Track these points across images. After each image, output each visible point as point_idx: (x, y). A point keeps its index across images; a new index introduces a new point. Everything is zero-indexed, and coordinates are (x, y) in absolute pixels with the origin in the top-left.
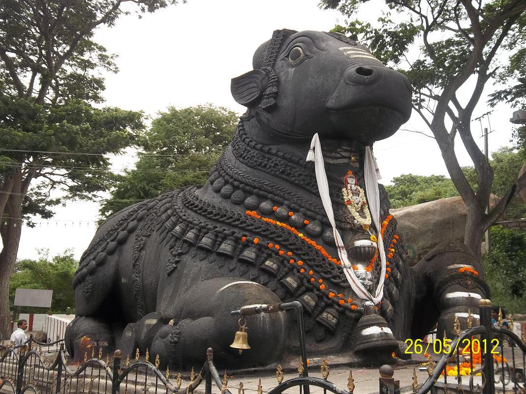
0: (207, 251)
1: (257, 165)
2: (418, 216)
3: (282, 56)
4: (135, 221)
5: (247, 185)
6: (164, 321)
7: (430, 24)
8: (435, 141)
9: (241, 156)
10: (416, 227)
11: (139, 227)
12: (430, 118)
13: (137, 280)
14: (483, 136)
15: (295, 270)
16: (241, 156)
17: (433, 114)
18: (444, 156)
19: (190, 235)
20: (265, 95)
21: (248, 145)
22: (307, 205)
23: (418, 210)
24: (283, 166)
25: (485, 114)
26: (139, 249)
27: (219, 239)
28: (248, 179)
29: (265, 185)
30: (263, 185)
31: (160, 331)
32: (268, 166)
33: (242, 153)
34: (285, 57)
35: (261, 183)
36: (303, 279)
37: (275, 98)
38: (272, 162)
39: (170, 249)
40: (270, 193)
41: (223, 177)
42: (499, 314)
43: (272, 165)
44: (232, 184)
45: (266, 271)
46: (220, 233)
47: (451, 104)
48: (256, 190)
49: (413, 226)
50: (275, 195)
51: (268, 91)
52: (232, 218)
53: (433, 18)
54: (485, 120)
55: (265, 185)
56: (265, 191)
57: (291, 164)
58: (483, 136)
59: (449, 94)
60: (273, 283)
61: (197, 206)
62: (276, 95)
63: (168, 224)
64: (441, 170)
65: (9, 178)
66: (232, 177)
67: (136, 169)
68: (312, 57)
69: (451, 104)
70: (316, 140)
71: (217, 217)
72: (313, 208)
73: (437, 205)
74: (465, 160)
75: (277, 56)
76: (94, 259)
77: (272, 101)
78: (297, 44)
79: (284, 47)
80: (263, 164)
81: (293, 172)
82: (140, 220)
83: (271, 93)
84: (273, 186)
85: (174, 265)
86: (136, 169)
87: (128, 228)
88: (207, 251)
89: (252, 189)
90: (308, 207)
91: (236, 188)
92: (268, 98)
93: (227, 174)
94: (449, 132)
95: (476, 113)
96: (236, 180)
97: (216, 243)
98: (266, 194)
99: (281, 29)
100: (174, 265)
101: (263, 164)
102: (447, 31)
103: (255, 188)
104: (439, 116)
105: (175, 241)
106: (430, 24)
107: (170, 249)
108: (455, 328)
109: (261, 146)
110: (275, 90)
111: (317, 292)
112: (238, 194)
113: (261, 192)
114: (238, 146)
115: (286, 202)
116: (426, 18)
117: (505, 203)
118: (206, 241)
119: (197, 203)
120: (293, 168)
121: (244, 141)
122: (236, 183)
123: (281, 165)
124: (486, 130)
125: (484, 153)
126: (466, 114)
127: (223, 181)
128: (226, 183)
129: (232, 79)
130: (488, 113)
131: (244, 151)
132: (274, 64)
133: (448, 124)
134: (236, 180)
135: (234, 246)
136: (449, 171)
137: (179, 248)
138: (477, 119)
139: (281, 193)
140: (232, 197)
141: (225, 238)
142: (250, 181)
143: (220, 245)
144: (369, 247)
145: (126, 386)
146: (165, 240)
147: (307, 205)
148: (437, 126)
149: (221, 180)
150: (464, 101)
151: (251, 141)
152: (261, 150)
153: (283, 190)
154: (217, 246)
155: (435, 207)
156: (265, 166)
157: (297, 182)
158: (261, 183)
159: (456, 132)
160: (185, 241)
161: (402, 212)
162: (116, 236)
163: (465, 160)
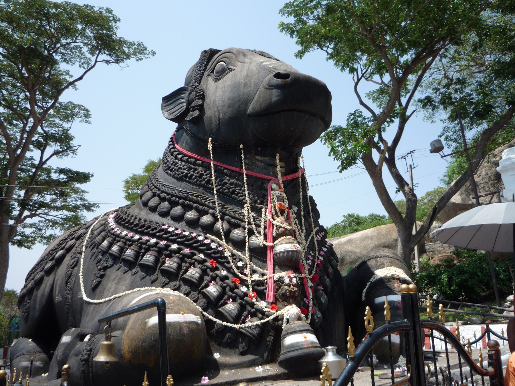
0: (148, 269)
1: (182, 176)
4: (74, 241)
5: (173, 196)
7: (359, 78)
9: (168, 169)
10: (357, 251)
11: (77, 245)
13: (68, 298)
14: (408, 172)
15: (218, 278)
19: (115, 248)
20: (191, 108)
21: (176, 158)
22: (231, 213)
24: (208, 176)
25: (408, 153)
26: (72, 266)
27: (143, 251)
28: (174, 190)
29: (190, 195)
30: (188, 195)
32: (117, 279)
33: (170, 165)
34: (211, 72)
35: (186, 193)
36: (226, 287)
38: (198, 173)
39: (97, 263)
40: (194, 202)
41: (151, 190)
43: (198, 175)
44: (159, 196)
48: (181, 201)
49: (355, 250)
53: (362, 73)
54: (409, 159)
55: (190, 195)
58: (408, 172)
61: (125, 220)
66: (159, 190)
67: (51, 175)
68: (234, 70)
72: (237, 215)
75: (203, 74)
78: (223, 59)
82: (78, 238)
84: (198, 196)
85: (99, 279)
86: (51, 175)
87: (66, 247)
88: (130, 264)
89: (177, 199)
90: (233, 215)
91: (163, 200)
93: (155, 187)
94: (377, 164)
96: (163, 192)
100: (99, 279)
103: (180, 198)
106: (359, 78)
107: (97, 263)
108: (366, 323)
111: (239, 301)
112: (166, 205)
114: (167, 159)
115: (211, 211)
118: (149, 258)
119: (125, 217)
121: (172, 155)
122: (163, 195)
123: (206, 175)
125: (384, 164)
126: (392, 150)
128: (154, 195)
131: (172, 164)
132: (200, 80)
135: (136, 251)
136: (386, 209)
137: (105, 262)
138: (403, 157)
139: (207, 203)
140: (158, 208)
141: (147, 250)
142: (177, 192)
143: (143, 257)
146: (95, 255)
147: (231, 213)
149: (156, 199)
151: (178, 154)
153: (204, 198)
154: (140, 258)
157: (309, 262)
158: (186, 193)
160: (111, 255)
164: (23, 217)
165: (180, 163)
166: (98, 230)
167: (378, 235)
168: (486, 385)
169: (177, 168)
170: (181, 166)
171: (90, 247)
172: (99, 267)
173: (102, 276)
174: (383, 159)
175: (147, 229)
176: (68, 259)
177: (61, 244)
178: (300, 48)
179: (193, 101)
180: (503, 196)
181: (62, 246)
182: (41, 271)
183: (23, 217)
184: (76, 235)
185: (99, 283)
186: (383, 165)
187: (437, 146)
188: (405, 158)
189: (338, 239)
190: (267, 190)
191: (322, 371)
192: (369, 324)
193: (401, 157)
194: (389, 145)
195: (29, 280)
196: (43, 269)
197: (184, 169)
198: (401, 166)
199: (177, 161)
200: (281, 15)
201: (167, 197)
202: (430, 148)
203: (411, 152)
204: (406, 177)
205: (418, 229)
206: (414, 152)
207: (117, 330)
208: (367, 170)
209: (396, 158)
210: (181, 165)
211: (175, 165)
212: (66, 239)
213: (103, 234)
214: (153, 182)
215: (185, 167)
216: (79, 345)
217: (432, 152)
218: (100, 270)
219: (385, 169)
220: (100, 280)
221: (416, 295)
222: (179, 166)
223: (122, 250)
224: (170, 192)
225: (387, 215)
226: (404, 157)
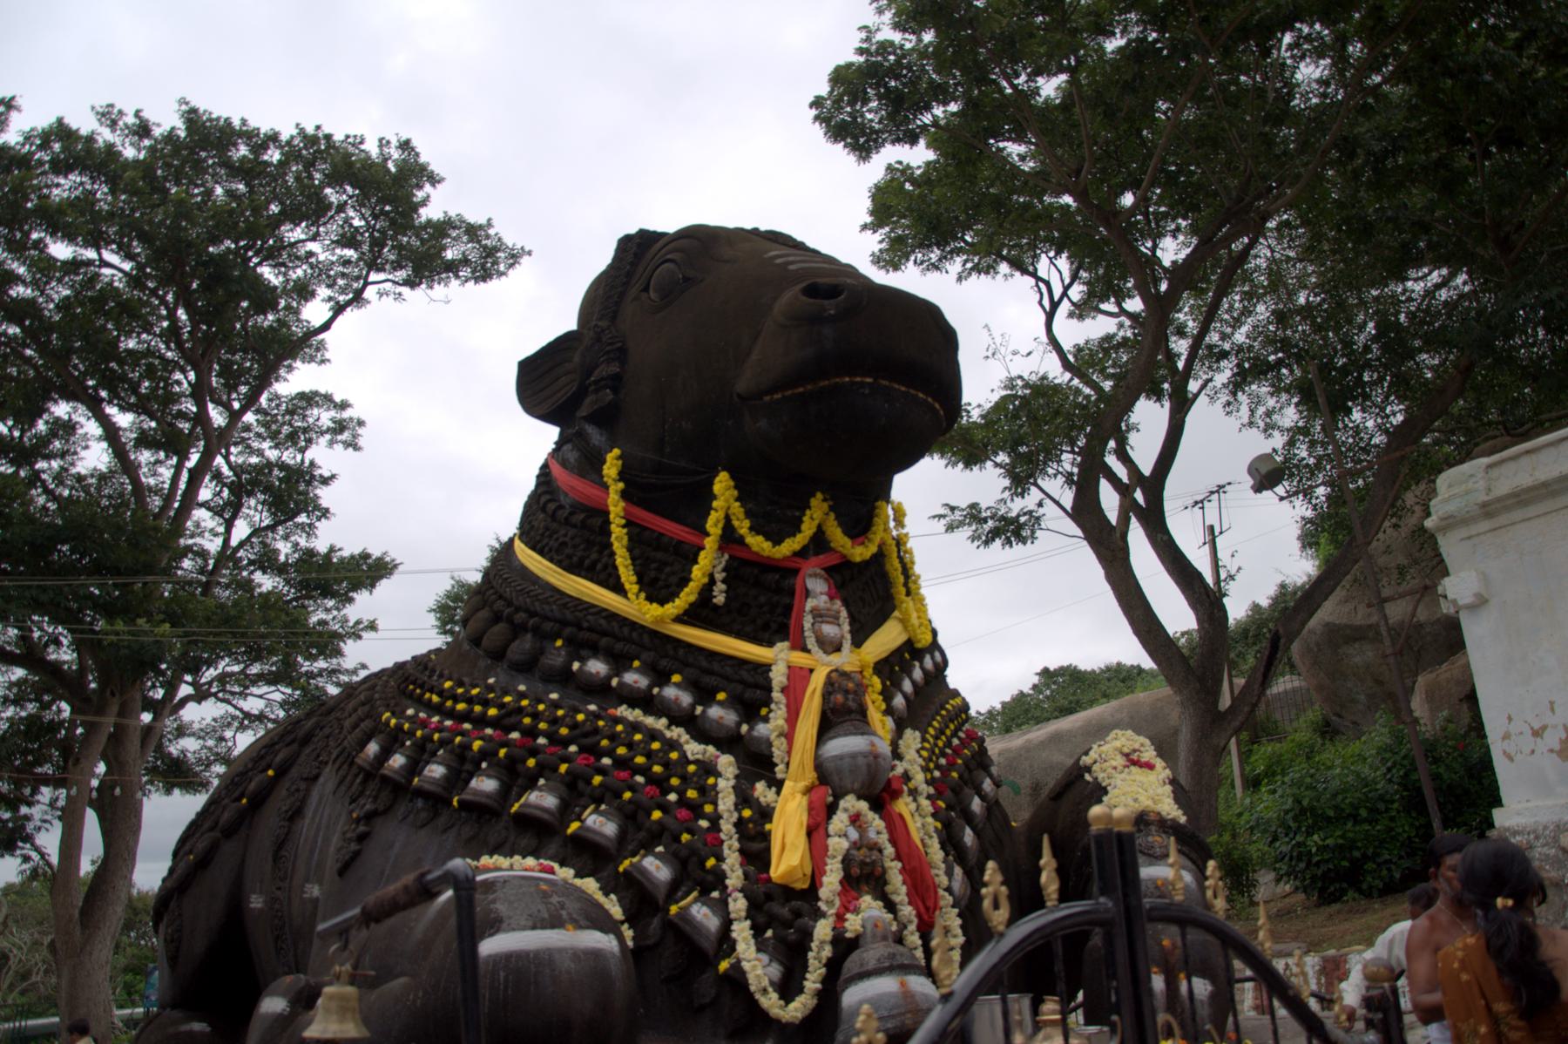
3: (633, 291)
4: (295, 746)
7: (1056, 298)
18: (1110, 578)
23: (1079, 724)
25: (1212, 493)
28: (548, 603)
32: (599, 566)
37: (615, 390)
40: (604, 634)
42: (1260, 922)
50: (618, 639)
54: (1211, 508)
56: (590, 629)
57: (659, 555)
62: (616, 382)
64: (1131, 652)
65: (108, 693)
66: (509, 604)
70: (722, 484)
74: (1177, 616)
77: (608, 395)
78: (669, 257)
79: (640, 269)
80: (587, 562)
81: (663, 577)
83: (602, 379)
93: (501, 597)
94: (1114, 521)
98: (594, 636)
101: (587, 562)
102: (1101, 317)
105: (365, 781)
106: (1056, 298)
109: (582, 516)
110: (614, 368)
116: (1047, 284)
120: (666, 564)
126: (1155, 484)
128: (497, 618)
130: (1220, 487)
133: (1109, 500)
138: (1196, 503)
144: (865, 755)
148: (1086, 512)
149: (500, 628)
150: (1144, 449)
152: (584, 525)
158: (581, 611)
159: (1129, 519)
160: (386, 780)
161: (1042, 732)
163: (1177, 616)
164: (177, 698)
165: (563, 532)
166: (354, 717)
167: (1132, 718)
169: (556, 545)
170: (567, 539)
171: (334, 762)
172: (355, 815)
173: (362, 838)
174: (1128, 507)
176: (282, 792)
177: (262, 757)
178: (869, 219)
179: (597, 366)
180: (1445, 597)
182: (212, 829)
183: (177, 698)
184: (301, 733)
185: (356, 855)
186: (1131, 527)
187: (1264, 470)
188: (1202, 508)
189: (1024, 734)
190: (792, 593)
191: (858, 1025)
192: (996, 906)
193: (1191, 502)
194: (1146, 469)
195: (182, 853)
196: (217, 823)
198: (1186, 532)
199: (555, 525)
200: (310, 130)
203: (1220, 489)
204: (1199, 559)
206: (1227, 488)
207: (397, 976)
208: (1086, 538)
210: (565, 535)
211: (550, 536)
212: (273, 745)
214: (494, 584)
215: (577, 540)
217: (1258, 488)
218: (358, 820)
219: (1137, 538)
220: (357, 847)
221: (1131, 836)
222: (561, 540)
223: (414, 767)
224: (538, 609)
225: (1148, 663)
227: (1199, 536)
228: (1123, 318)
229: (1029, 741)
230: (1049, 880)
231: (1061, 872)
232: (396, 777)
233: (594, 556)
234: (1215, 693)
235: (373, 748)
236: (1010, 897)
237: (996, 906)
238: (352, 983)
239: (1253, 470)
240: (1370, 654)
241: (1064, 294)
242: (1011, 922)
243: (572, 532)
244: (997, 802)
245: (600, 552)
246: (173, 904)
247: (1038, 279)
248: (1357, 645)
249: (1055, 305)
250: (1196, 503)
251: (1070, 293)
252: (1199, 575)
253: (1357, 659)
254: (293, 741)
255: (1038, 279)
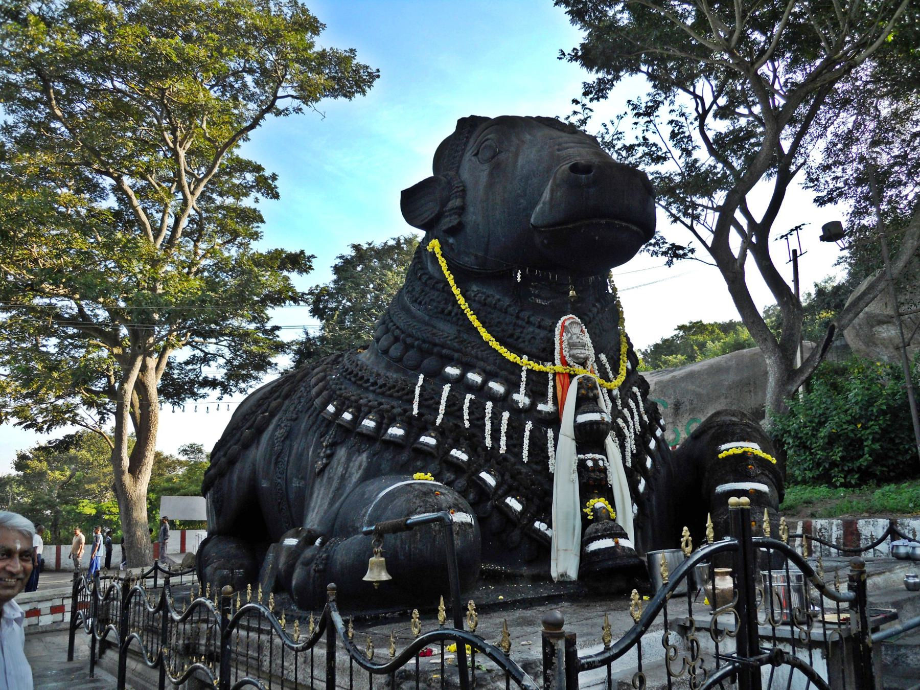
2: (706, 377)
6: (309, 540)
7: (707, 107)
8: (717, 270)
12: (709, 239)
16: (416, 301)
17: (712, 231)
18: (731, 290)
25: (792, 230)
31: (303, 556)
32: (453, 314)
37: (460, 215)
40: (457, 351)
45: (455, 465)
46: (387, 411)
47: (738, 215)
49: (698, 390)
51: (451, 204)
52: (403, 389)
54: (793, 239)
56: (449, 348)
59: (737, 199)
60: (461, 482)
63: (317, 402)
64: (730, 313)
69: (738, 215)
71: (383, 389)
73: (730, 359)
76: (225, 455)
80: (446, 311)
92: (451, 215)
93: (398, 328)
94: (736, 257)
95: (778, 228)
97: (382, 426)
99: (467, 116)
101: (446, 311)
103: (435, 345)
104: (721, 234)
106: (707, 107)
113: (444, 351)
116: (702, 99)
117: (820, 352)
119: (356, 370)
122: (409, 340)
124: (795, 251)
125: (749, 252)
126: (762, 229)
127: (392, 339)
128: (396, 339)
129: (402, 192)
133: (735, 241)
134: (410, 336)
138: (782, 237)
140: (404, 359)
145: (248, 637)
148: (719, 249)
154: (383, 431)
155: (730, 363)
156: (450, 313)
162: (254, 422)
168: (847, 687)
174: (747, 244)
175: (390, 389)
181: (265, 407)
192: (687, 546)
194: (758, 218)
197: (439, 302)
201: (416, 343)
202: (822, 234)
203: (797, 228)
205: (806, 355)
209: (770, 239)
213: (325, 393)
216: (308, 553)
217: (823, 239)
223: (357, 420)
226: (785, 237)
227: (786, 256)
228: (751, 119)
229: (674, 377)
230: (710, 532)
231: (714, 528)
232: (348, 426)
233: (450, 308)
234: (792, 360)
235: (331, 408)
236: (692, 541)
237: (687, 546)
238: (382, 556)
239: (826, 228)
240: (893, 332)
241: (714, 102)
242: (693, 551)
243: (437, 293)
244: (664, 440)
245: (453, 306)
246: (216, 482)
247: (696, 97)
248: (885, 326)
249: (706, 112)
250: (782, 237)
251: (718, 101)
252: (789, 288)
253: (885, 335)
254: (278, 397)
255: (696, 97)
